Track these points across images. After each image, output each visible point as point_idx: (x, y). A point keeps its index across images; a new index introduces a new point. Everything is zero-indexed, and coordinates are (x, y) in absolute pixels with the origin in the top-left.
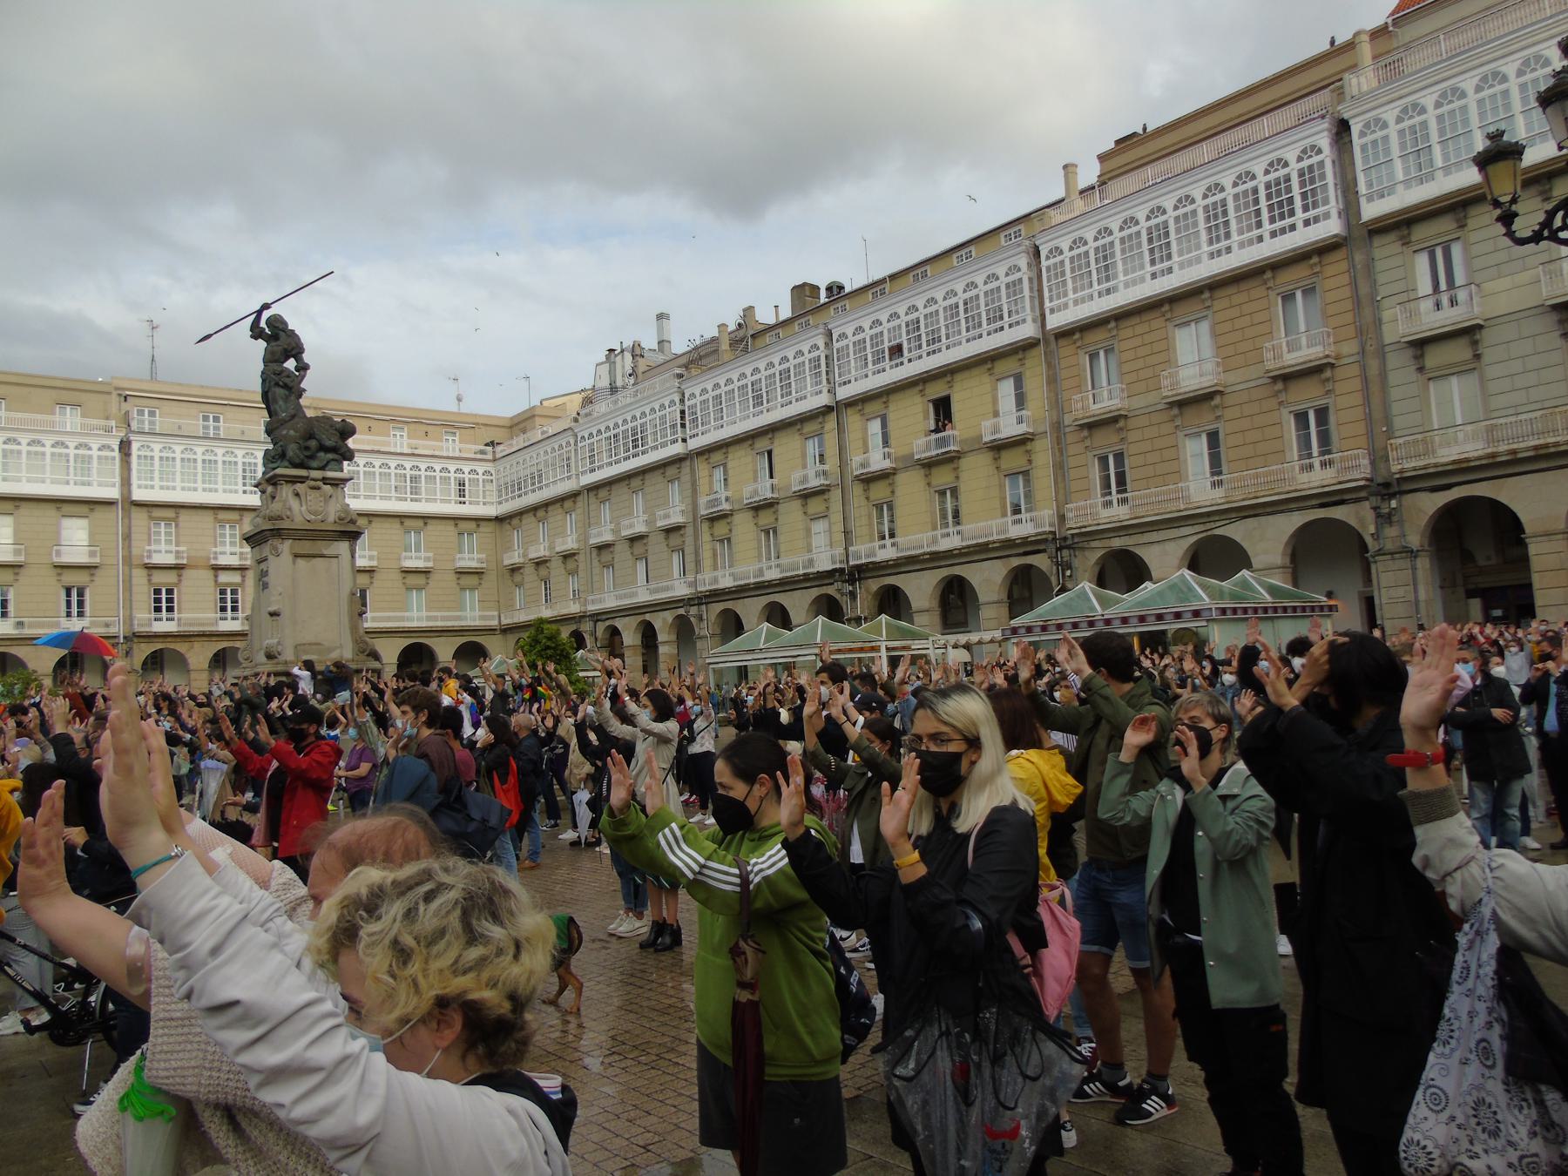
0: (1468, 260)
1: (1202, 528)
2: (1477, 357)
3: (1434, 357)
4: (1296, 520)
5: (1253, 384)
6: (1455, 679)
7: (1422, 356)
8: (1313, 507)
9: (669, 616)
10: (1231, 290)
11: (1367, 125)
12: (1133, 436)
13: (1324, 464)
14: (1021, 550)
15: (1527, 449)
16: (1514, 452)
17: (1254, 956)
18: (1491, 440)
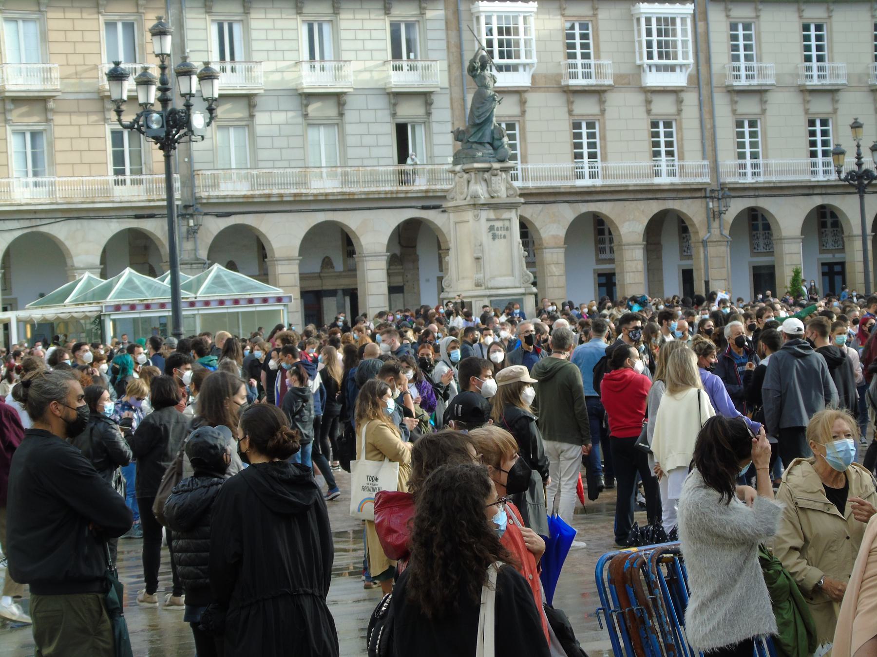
1: (27, 223)
3: (314, 108)
4: (115, 227)
5: (81, 96)
6: (830, 340)
8: (129, 217)
9: (568, 213)
12: (58, 119)
14: (420, 204)
15: (290, 195)
16: (281, 196)
18: (344, 183)
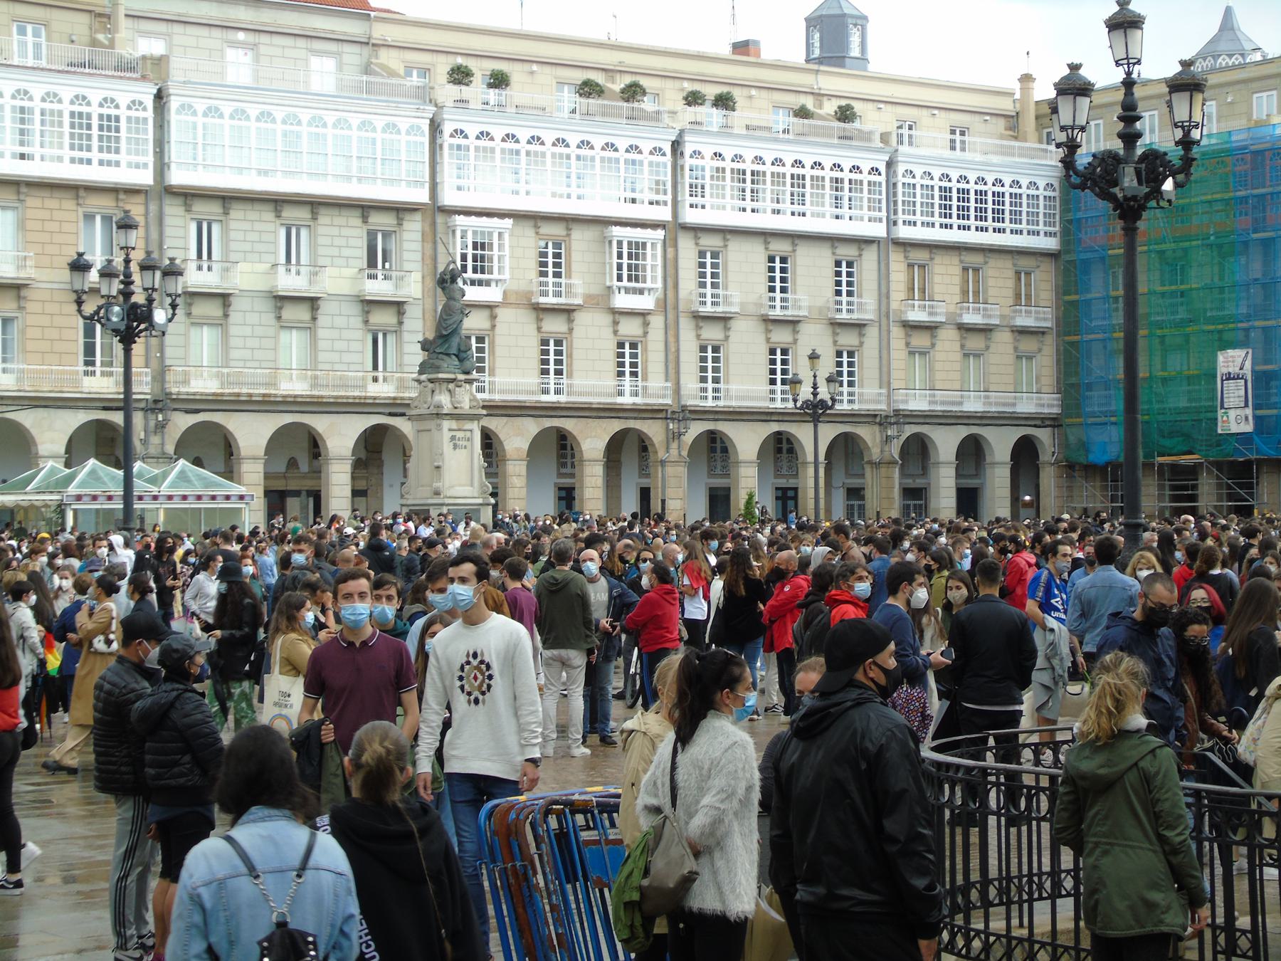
0: (313, 246)
2: (226, 316)
4: (616, 426)
7: (281, 308)
9: (532, 427)
10: (46, 193)
11: (182, 106)
13: (103, 374)
15: (259, 395)
17: (704, 772)
18: (313, 386)
